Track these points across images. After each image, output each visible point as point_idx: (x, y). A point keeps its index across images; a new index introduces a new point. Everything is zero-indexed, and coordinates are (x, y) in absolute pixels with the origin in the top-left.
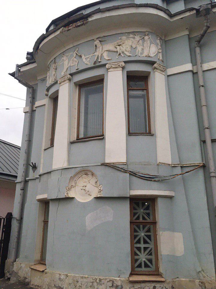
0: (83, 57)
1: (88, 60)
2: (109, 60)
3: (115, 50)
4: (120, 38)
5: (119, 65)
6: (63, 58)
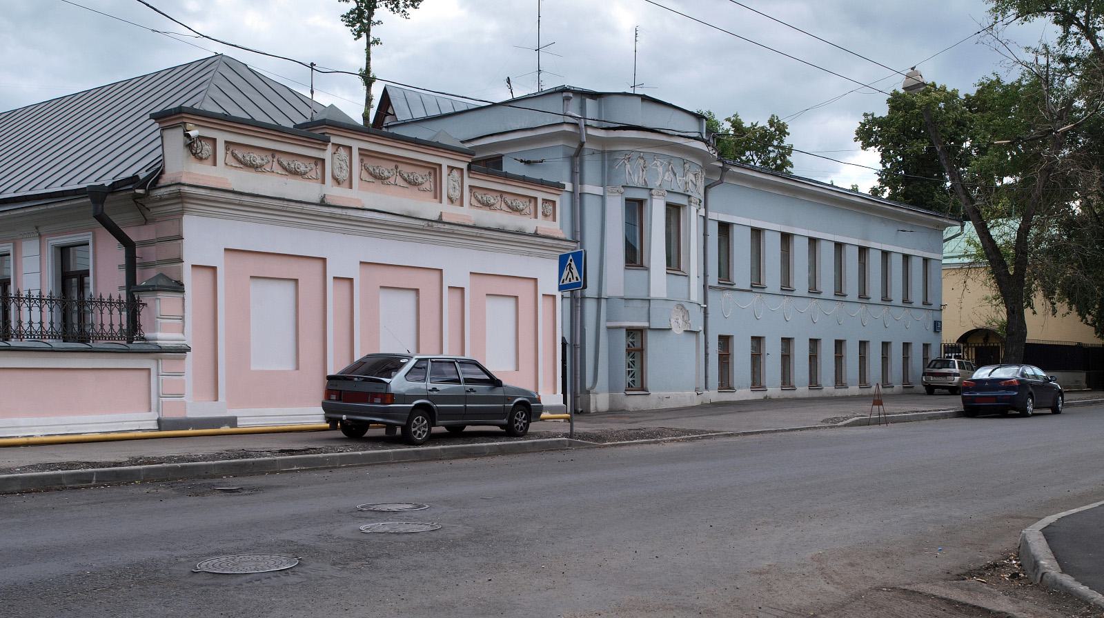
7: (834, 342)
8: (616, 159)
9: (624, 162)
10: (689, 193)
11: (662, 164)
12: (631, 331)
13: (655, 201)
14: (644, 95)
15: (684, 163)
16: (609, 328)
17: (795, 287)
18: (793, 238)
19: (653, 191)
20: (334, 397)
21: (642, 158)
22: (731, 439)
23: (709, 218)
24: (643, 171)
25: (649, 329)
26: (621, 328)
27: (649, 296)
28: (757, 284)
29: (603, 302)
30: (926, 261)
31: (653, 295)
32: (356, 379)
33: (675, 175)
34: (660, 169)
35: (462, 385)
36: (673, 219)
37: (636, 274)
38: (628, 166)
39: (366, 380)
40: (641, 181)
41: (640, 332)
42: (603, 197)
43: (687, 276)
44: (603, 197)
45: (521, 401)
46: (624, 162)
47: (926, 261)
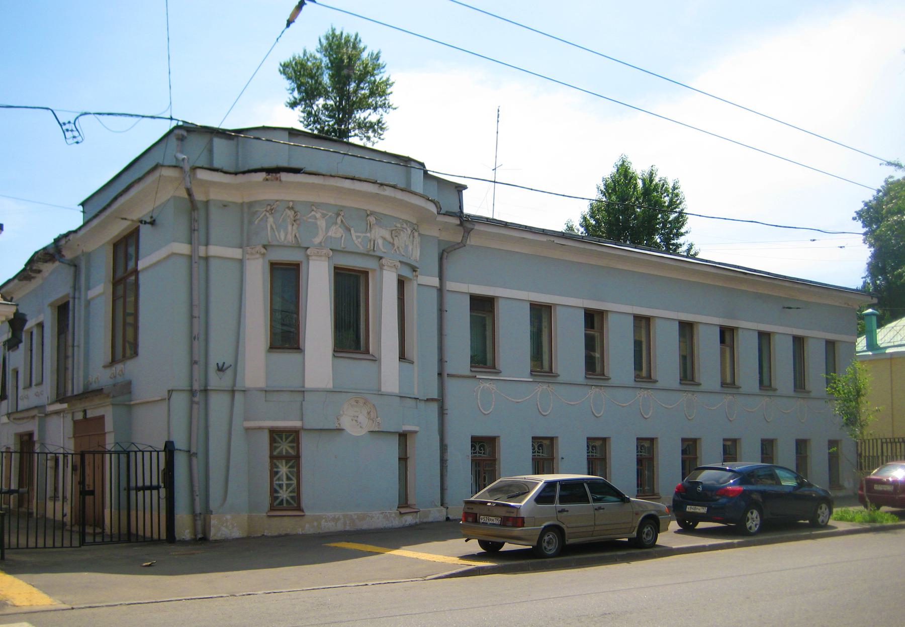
0: (352, 231)
1: (360, 240)
2: (385, 252)
3: (392, 241)
4: (394, 223)
5: (395, 265)
6: (313, 213)
7: (760, 442)
8: (257, 211)
9: (265, 215)
10: (378, 254)
11: (324, 216)
12: (276, 435)
13: (312, 264)
14: (292, 129)
15: (368, 215)
16: (247, 429)
17: (658, 378)
18: (738, 331)
19: (383, 261)
20: (470, 519)
21: (292, 208)
22: (379, 582)
23: (447, 289)
24: (293, 225)
25: (302, 428)
26: (260, 428)
27: (303, 387)
28: (729, 384)
29: (238, 397)
30: (830, 345)
31: (309, 384)
32: (489, 504)
33: (348, 230)
34: (322, 223)
35: (591, 504)
36: (121, 254)
37: (286, 358)
38: (271, 220)
39: (498, 504)
40: (290, 238)
41: (294, 435)
42: (241, 261)
43: (376, 360)
44: (241, 261)
45: (643, 519)
46: (265, 215)
47: (830, 345)
